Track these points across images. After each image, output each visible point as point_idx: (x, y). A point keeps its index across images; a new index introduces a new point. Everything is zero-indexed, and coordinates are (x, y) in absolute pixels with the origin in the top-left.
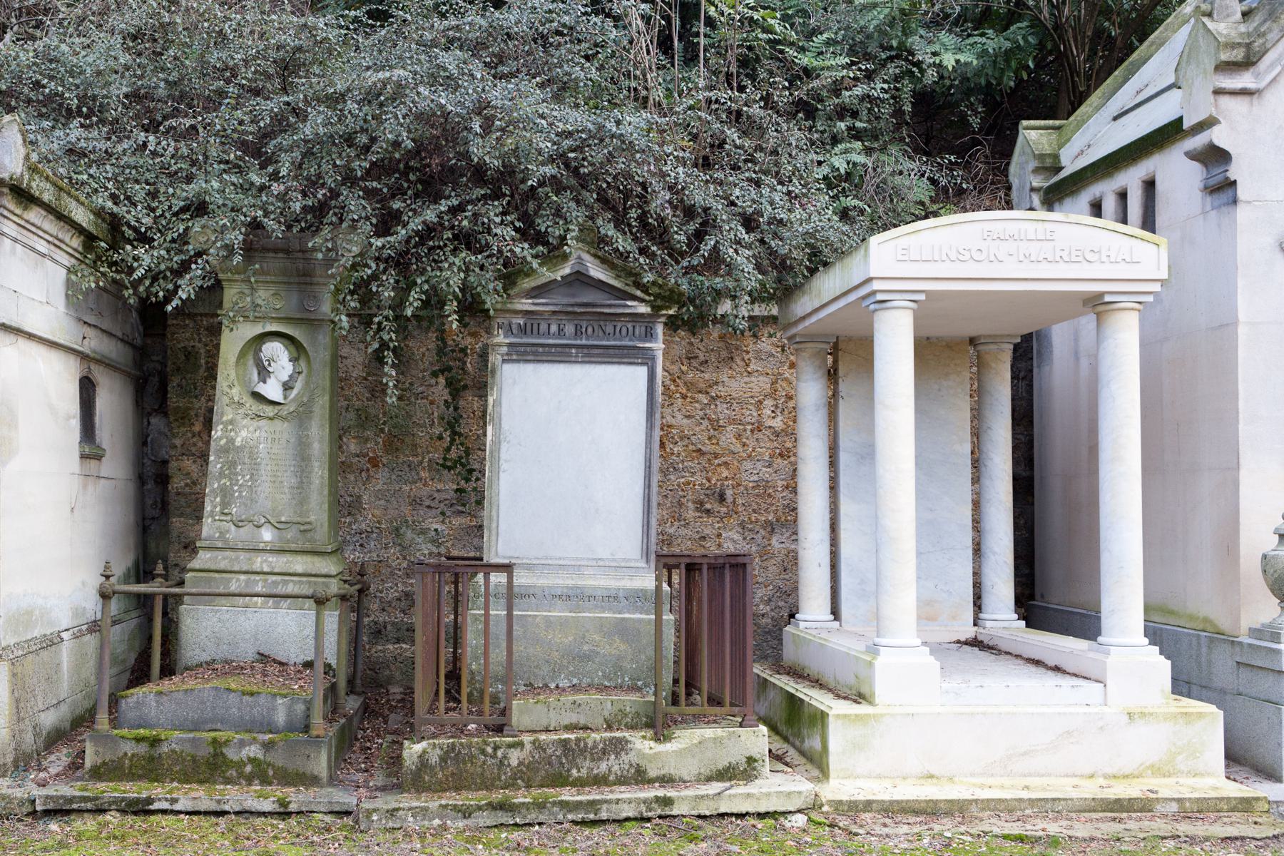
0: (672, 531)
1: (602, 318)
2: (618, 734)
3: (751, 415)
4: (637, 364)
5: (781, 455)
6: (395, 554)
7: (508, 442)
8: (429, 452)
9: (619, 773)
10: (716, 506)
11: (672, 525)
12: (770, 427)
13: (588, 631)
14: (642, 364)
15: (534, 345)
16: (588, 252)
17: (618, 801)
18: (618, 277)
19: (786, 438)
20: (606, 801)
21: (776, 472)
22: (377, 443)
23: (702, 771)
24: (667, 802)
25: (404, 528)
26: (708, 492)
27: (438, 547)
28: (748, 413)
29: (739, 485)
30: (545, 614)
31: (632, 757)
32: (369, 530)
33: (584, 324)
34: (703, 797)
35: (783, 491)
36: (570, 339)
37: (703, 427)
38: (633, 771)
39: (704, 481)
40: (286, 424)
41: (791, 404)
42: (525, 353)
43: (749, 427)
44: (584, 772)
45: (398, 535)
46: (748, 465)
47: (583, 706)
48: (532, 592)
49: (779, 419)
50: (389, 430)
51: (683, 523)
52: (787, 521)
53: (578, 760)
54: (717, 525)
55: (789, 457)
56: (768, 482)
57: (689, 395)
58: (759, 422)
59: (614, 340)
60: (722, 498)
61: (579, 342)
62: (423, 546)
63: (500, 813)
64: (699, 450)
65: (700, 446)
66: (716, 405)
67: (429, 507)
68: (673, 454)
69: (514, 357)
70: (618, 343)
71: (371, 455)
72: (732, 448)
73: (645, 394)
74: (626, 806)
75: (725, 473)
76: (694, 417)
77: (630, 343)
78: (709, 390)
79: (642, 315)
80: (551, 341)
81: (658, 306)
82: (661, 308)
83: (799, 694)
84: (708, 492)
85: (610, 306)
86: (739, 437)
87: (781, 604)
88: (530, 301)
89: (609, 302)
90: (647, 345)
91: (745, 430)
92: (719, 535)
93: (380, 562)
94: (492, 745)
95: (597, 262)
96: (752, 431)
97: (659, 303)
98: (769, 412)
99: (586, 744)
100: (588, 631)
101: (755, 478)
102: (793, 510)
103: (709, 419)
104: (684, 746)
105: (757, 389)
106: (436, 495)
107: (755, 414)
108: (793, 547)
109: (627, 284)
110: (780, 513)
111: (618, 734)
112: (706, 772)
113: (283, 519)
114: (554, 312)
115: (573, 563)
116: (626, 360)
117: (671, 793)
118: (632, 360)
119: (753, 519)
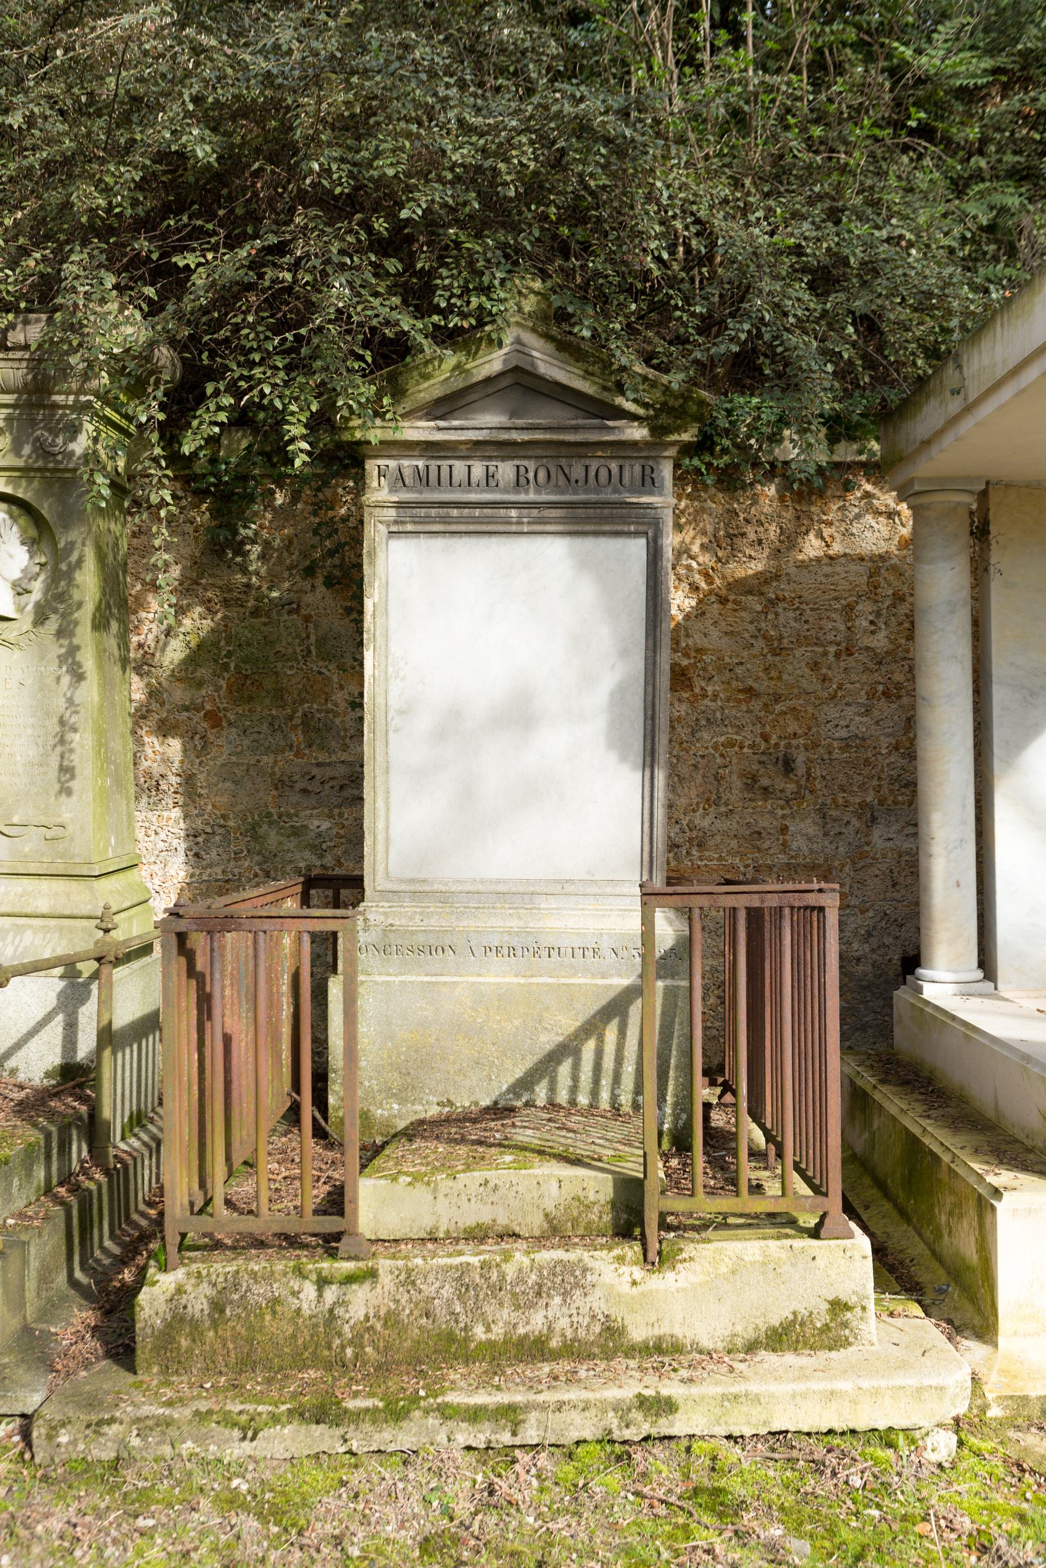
0: (705, 823)
1: (564, 451)
2: (572, 1256)
3: (835, 629)
4: (629, 534)
5: (886, 694)
6: (250, 868)
7: (403, 679)
8: (303, 701)
9: (569, 1334)
10: (780, 783)
11: (706, 814)
12: (867, 648)
13: (547, 1009)
14: (636, 534)
15: (443, 504)
16: (534, 330)
17: (560, 1406)
18: (588, 374)
19: (894, 666)
20: (543, 1407)
21: (877, 723)
22: (218, 689)
23: (739, 1329)
24: (666, 1406)
25: (265, 827)
26: (764, 758)
27: (321, 857)
28: (830, 625)
29: (816, 745)
30: (471, 979)
31: (597, 1302)
32: (209, 830)
33: (531, 465)
34: (736, 1397)
35: (890, 753)
36: (506, 491)
37: (755, 651)
38: (597, 1329)
39: (758, 740)
40: (17, 654)
41: (903, 609)
42: (428, 520)
43: (832, 649)
44: (498, 1332)
45: (255, 837)
46: (831, 711)
47: (502, 1191)
48: (447, 942)
49: (882, 634)
50: (237, 666)
51: (723, 809)
52: (895, 803)
53: (486, 1308)
54: (780, 812)
55: (899, 697)
56: (864, 739)
57: (732, 597)
58: (848, 640)
59: (586, 492)
60: (787, 766)
61: (522, 497)
62: (298, 856)
63: (318, 1430)
64: (749, 690)
65: (750, 682)
66: (777, 614)
67: (305, 791)
68: (705, 696)
69: (409, 527)
70: (593, 497)
71: (208, 707)
72: (804, 684)
73: (643, 589)
74: (575, 1416)
75: (793, 727)
76: (739, 633)
77: (615, 497)
78: (765, 589)
79: (634, 444)
80: (473, 497)
81: (662, 427)
82: (667, 430)
83: (926, 1140)
84: (764, 758)
85: (576, 429)
86: (815, 666)
87: (888, 940)
88: (432, 424)
89: (573, 422)
90: (645, 499)
91: (825, 654)
92: (784, 830)
93: (227, 881)
94: (314, 1277)
95: (550, 347)
96: (837, 655)
97: (664, 420)
98: (865, 624)
99: (502, 1277)
100: (547, 1009)
101: (843, 733)
102: (906, 786)
103: (764, 637)
104: (701, 1278)
105: (843, 585)
106: (315, 771)
107: (842, 627)
108: (906, 846)
109: (605, 388)
110: (885, 791)
111: (572, 1256)
112: (745, 1331)
113: (15, 820)
114: (478, 443)
115: (521, 890)
116: (607, 528)
117: (671, 1389)
118: (619, 528)
119: (841, 801)
